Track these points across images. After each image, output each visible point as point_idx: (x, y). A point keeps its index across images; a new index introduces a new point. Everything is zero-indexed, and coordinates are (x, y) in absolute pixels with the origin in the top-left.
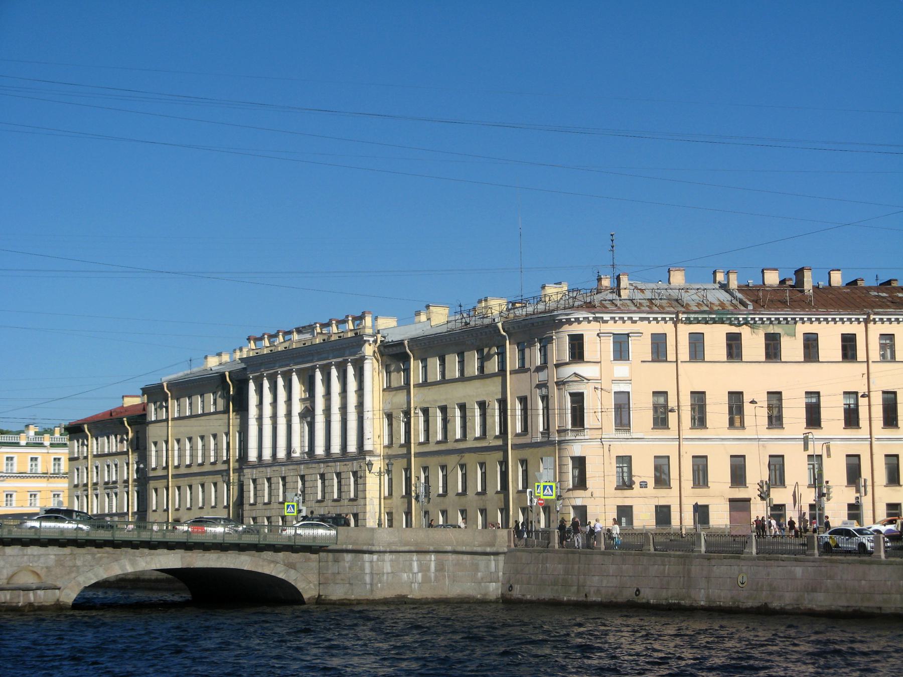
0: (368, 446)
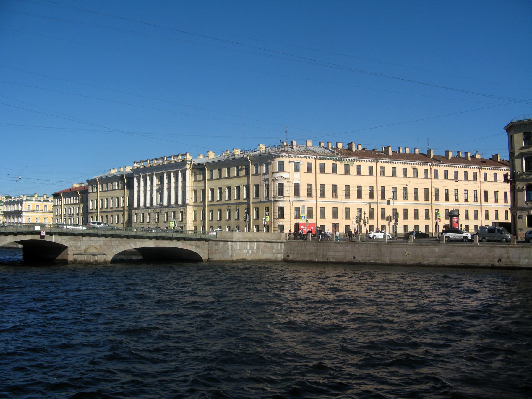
0: (187, 202)
